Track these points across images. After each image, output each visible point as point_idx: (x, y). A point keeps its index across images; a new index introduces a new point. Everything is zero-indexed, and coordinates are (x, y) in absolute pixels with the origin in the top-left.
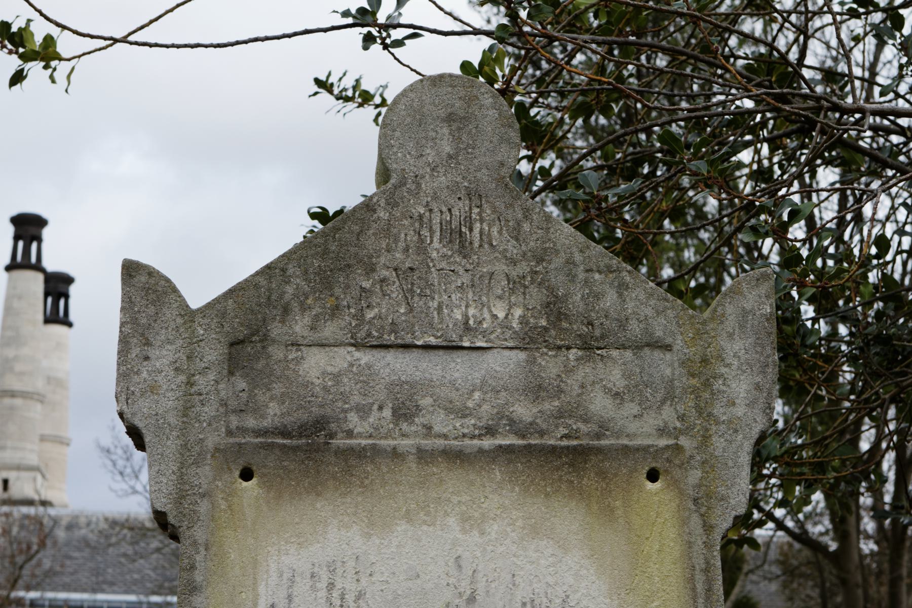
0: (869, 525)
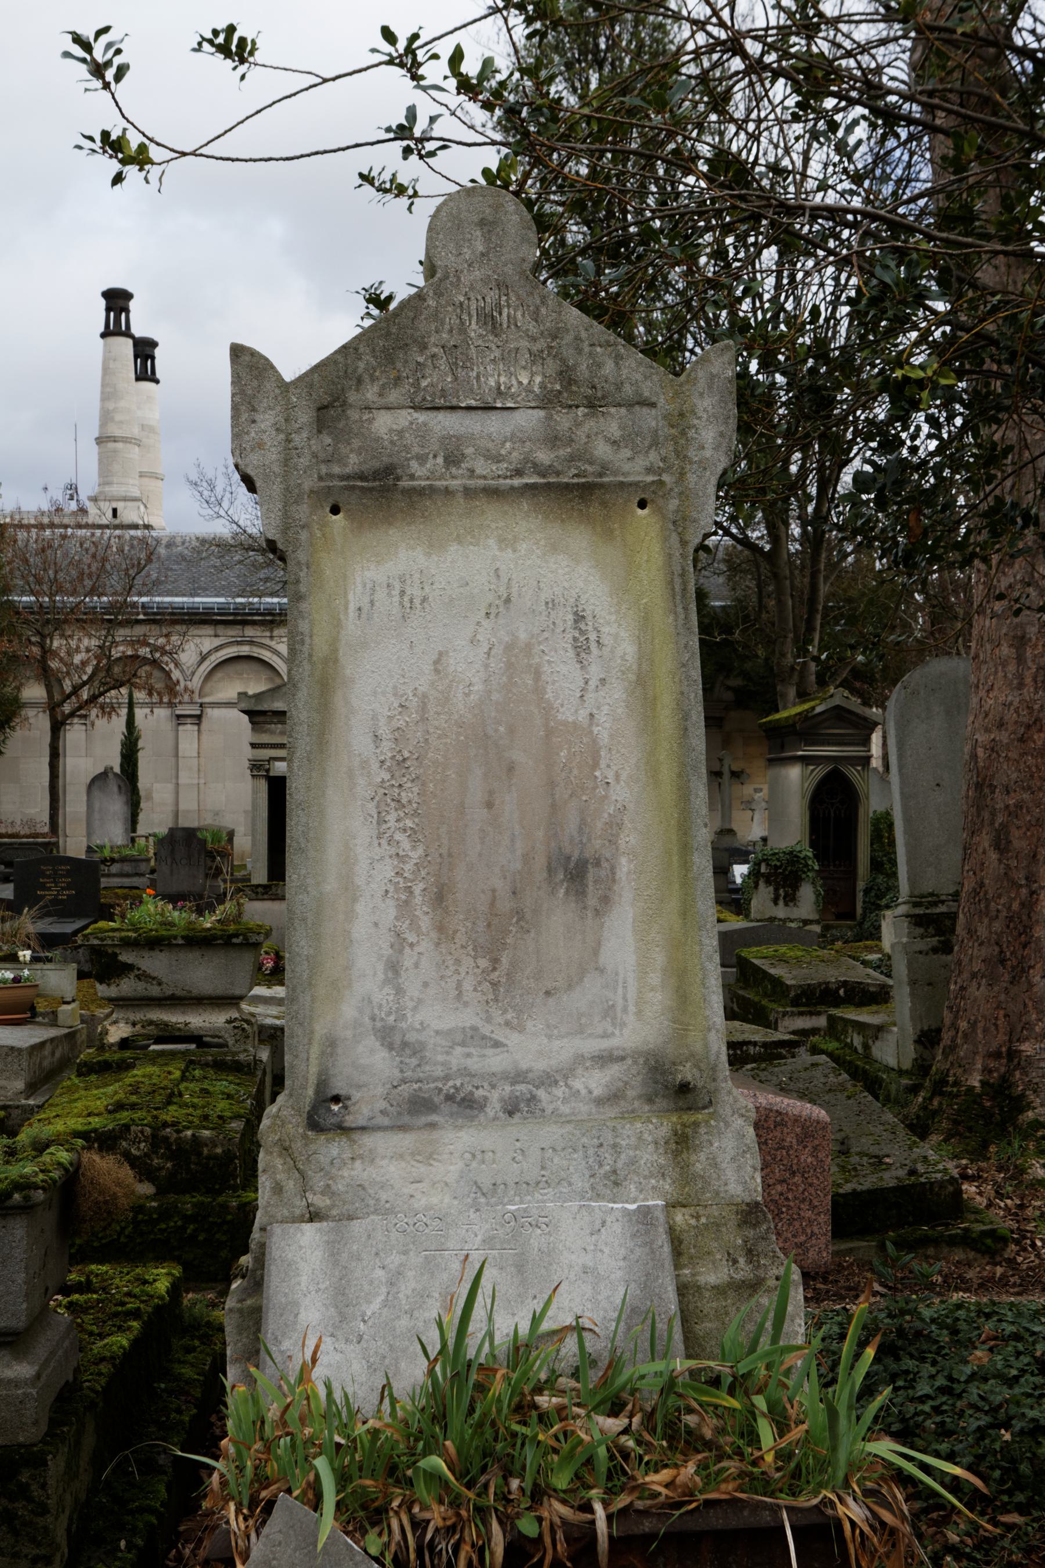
0: (796, 530)
